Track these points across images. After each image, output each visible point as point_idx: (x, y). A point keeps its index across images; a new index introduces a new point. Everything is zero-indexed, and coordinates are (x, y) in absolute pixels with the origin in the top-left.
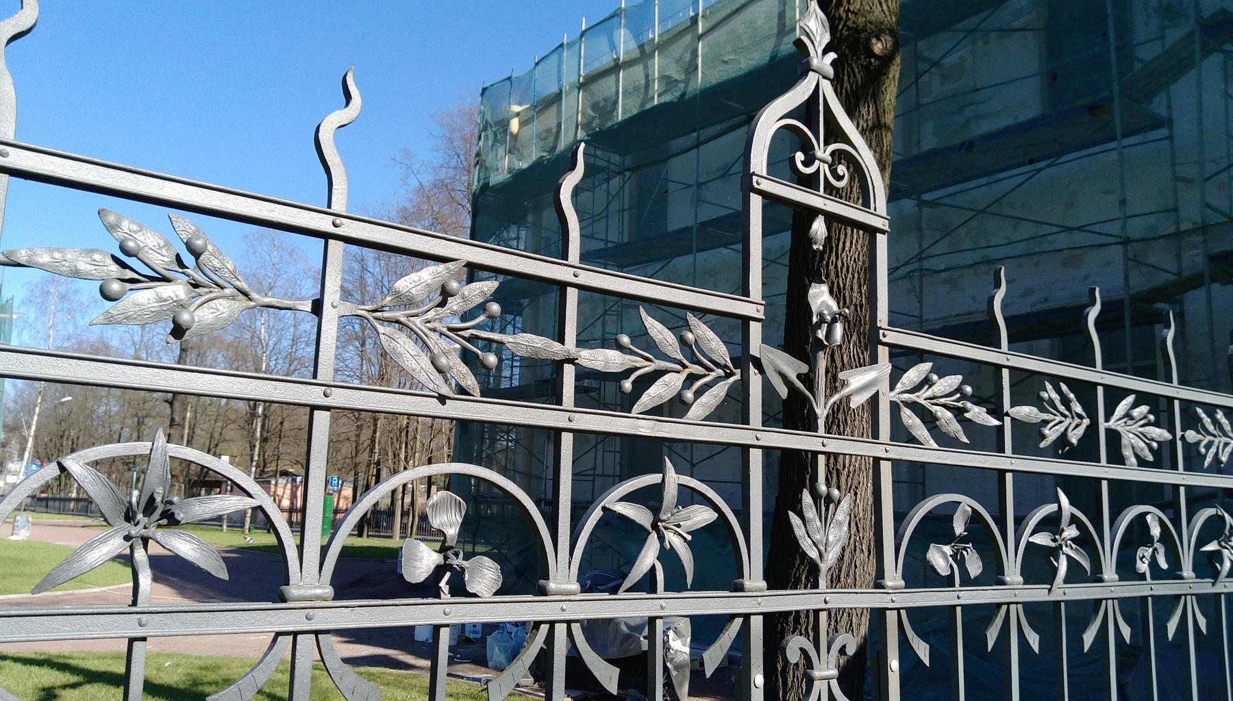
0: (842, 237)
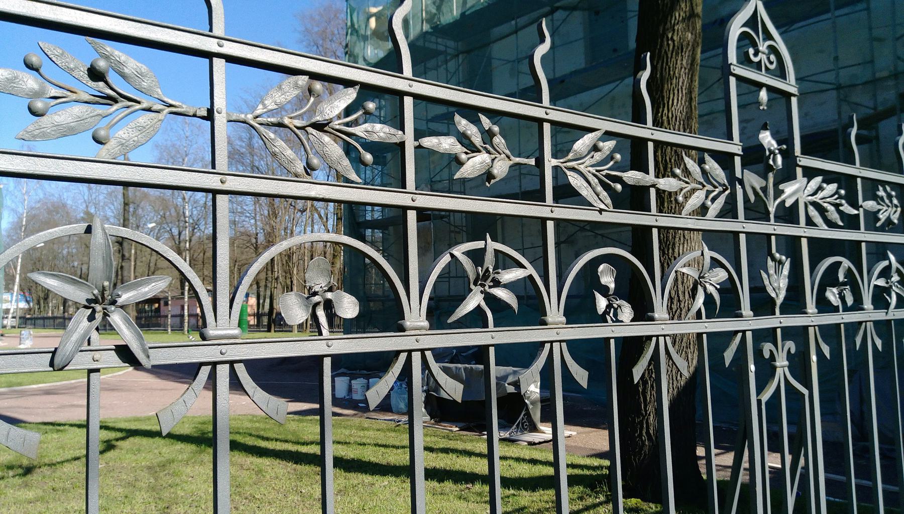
0: (671, 96)
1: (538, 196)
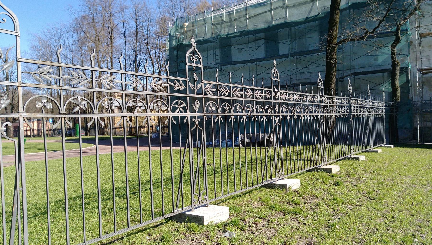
1: (201, 94)
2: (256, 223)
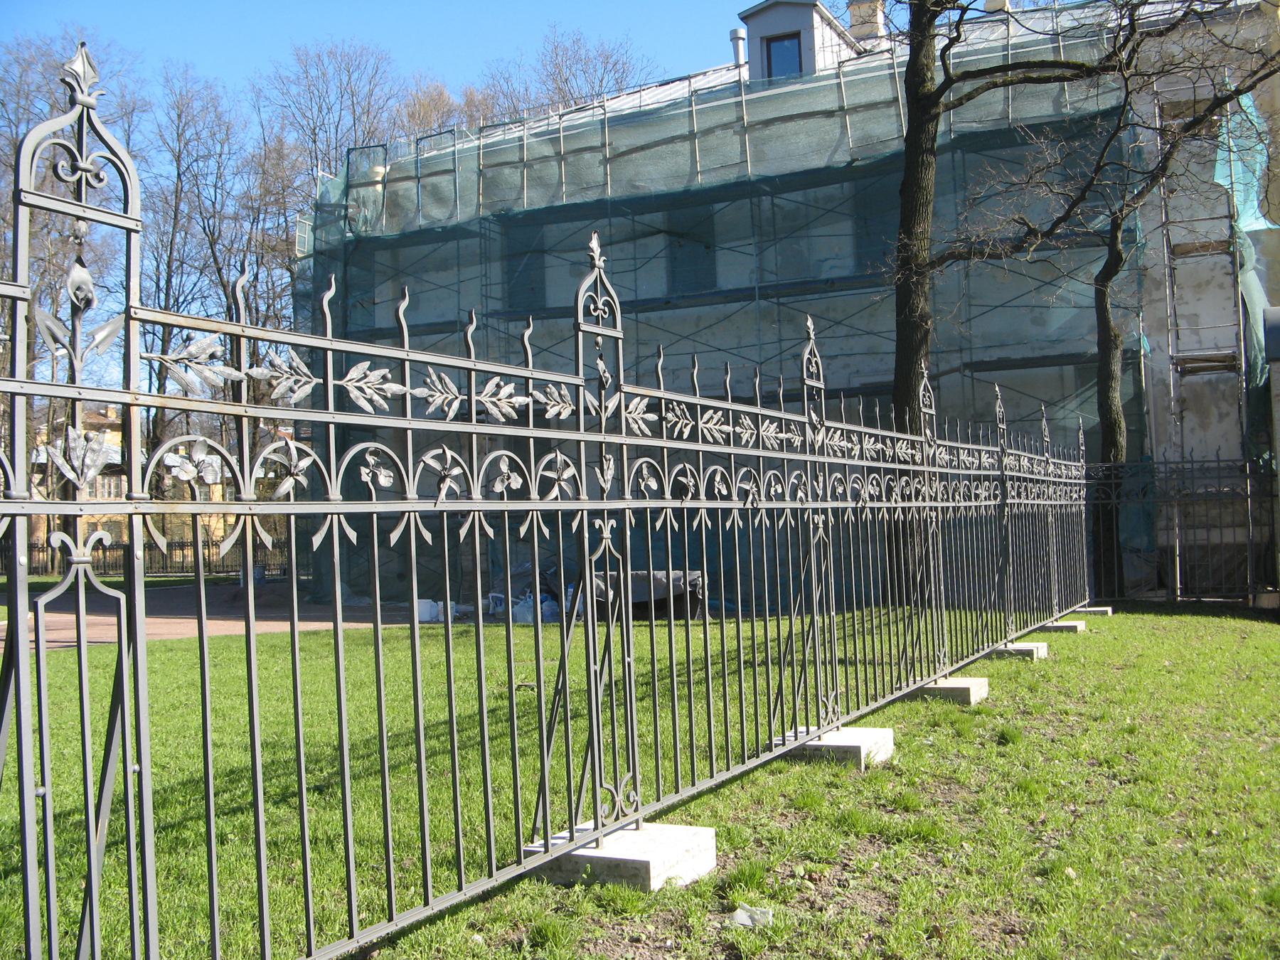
2: (814, 876)
